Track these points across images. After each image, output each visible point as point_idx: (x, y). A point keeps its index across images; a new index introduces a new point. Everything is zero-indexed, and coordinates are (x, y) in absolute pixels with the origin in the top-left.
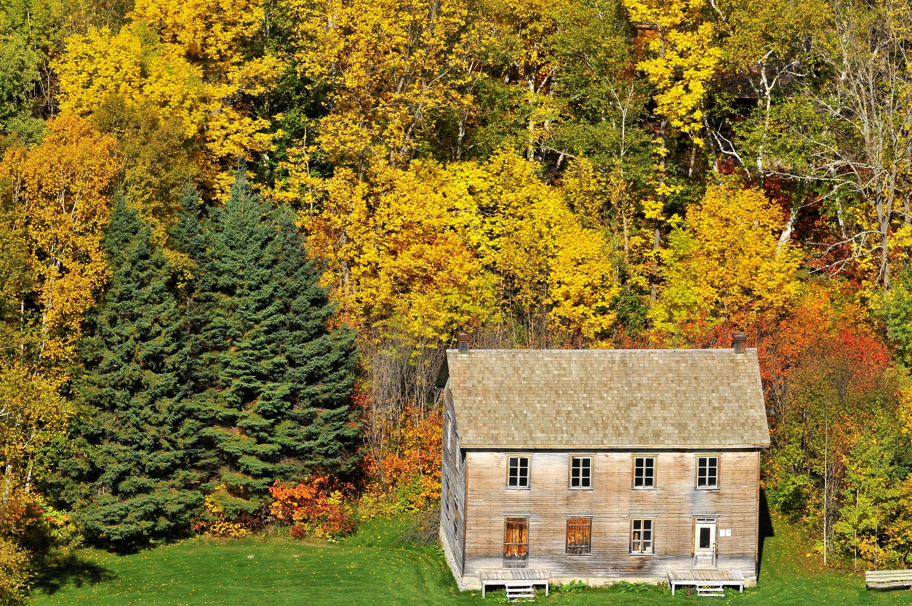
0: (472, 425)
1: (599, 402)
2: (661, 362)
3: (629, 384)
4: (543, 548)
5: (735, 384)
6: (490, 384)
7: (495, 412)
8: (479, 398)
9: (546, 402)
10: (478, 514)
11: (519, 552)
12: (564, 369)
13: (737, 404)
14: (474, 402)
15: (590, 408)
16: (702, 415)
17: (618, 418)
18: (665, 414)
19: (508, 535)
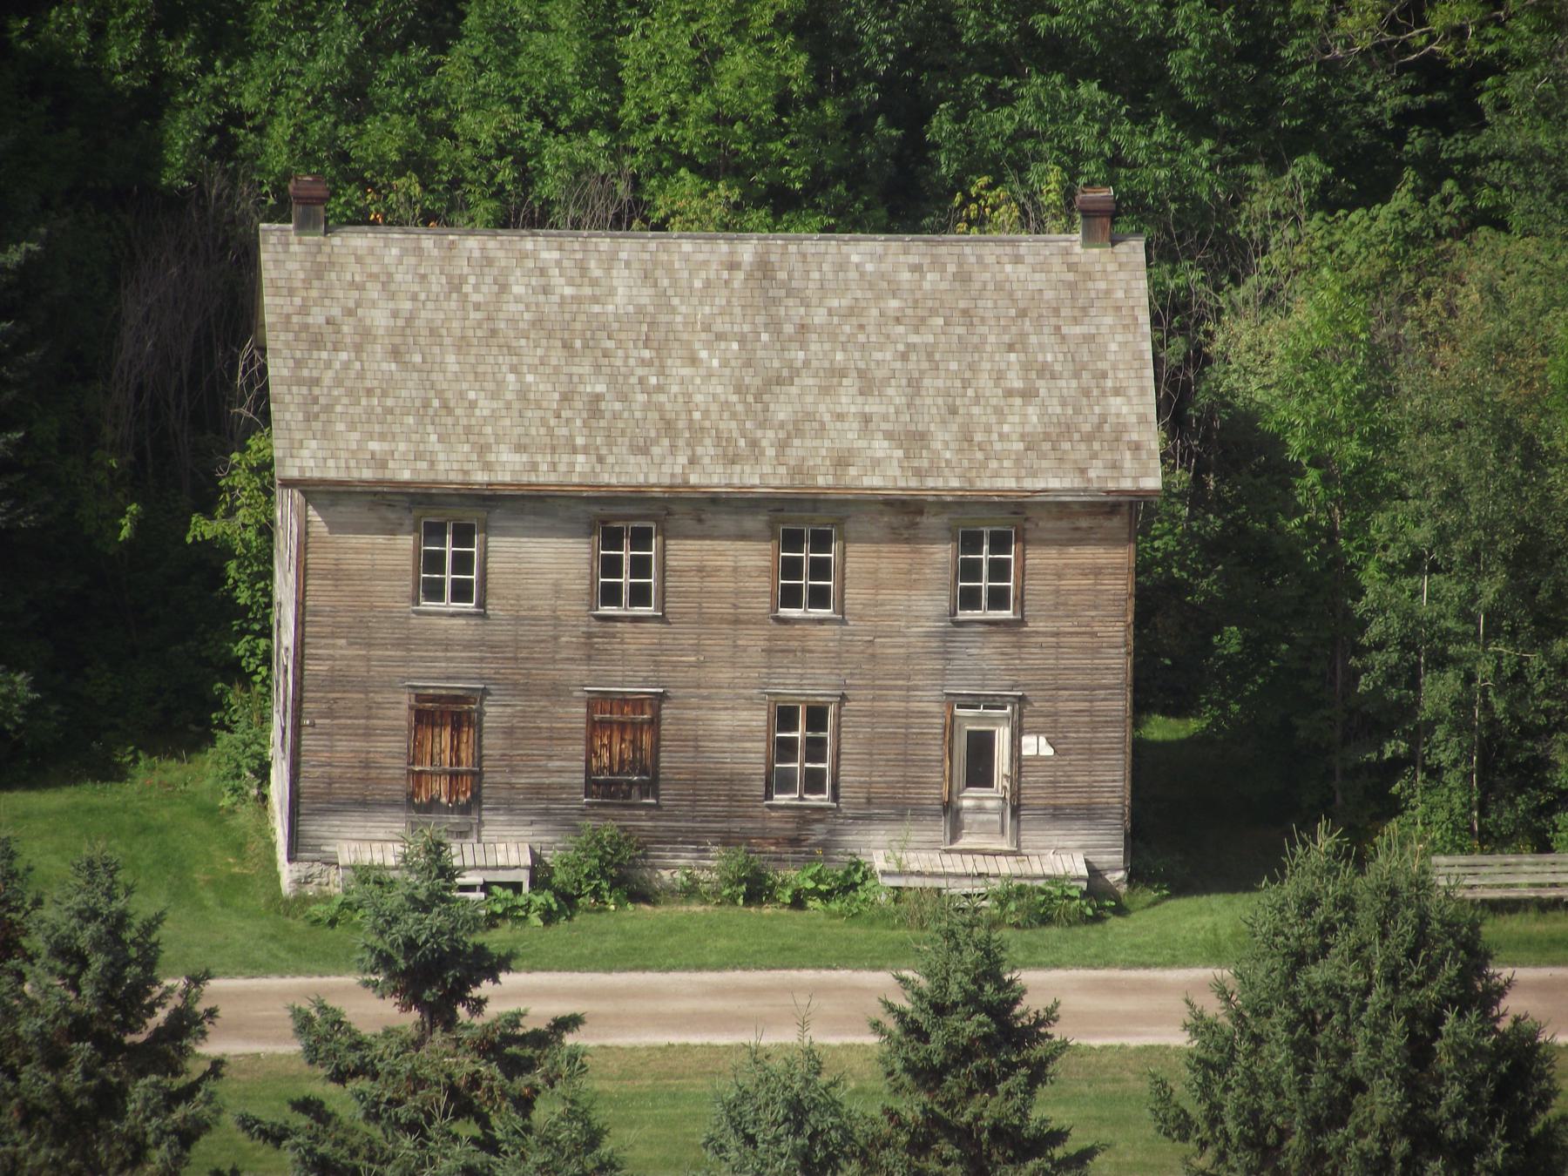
0: (317, 425)
1: (686, 371)
2: (869, 267)
3: (774, 326)
4: (522, 780)
5: (1078, 330)
6: (379, 318)
7: (384, 394)
8: (344, 356)
9: (533, 369)
10: (336, 681)
11: (452, 791)
12: (594, 283)
13: (1074, 383)
14: (328, 365)
15: (660, 389)
16: (975, 410)
17: (734, 416)
18: (873, 407)
19: (419, 745)
